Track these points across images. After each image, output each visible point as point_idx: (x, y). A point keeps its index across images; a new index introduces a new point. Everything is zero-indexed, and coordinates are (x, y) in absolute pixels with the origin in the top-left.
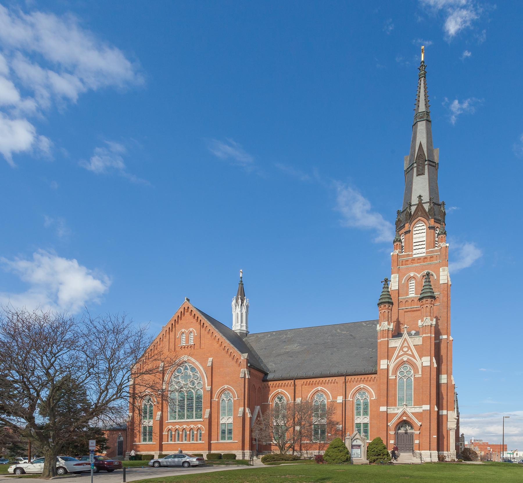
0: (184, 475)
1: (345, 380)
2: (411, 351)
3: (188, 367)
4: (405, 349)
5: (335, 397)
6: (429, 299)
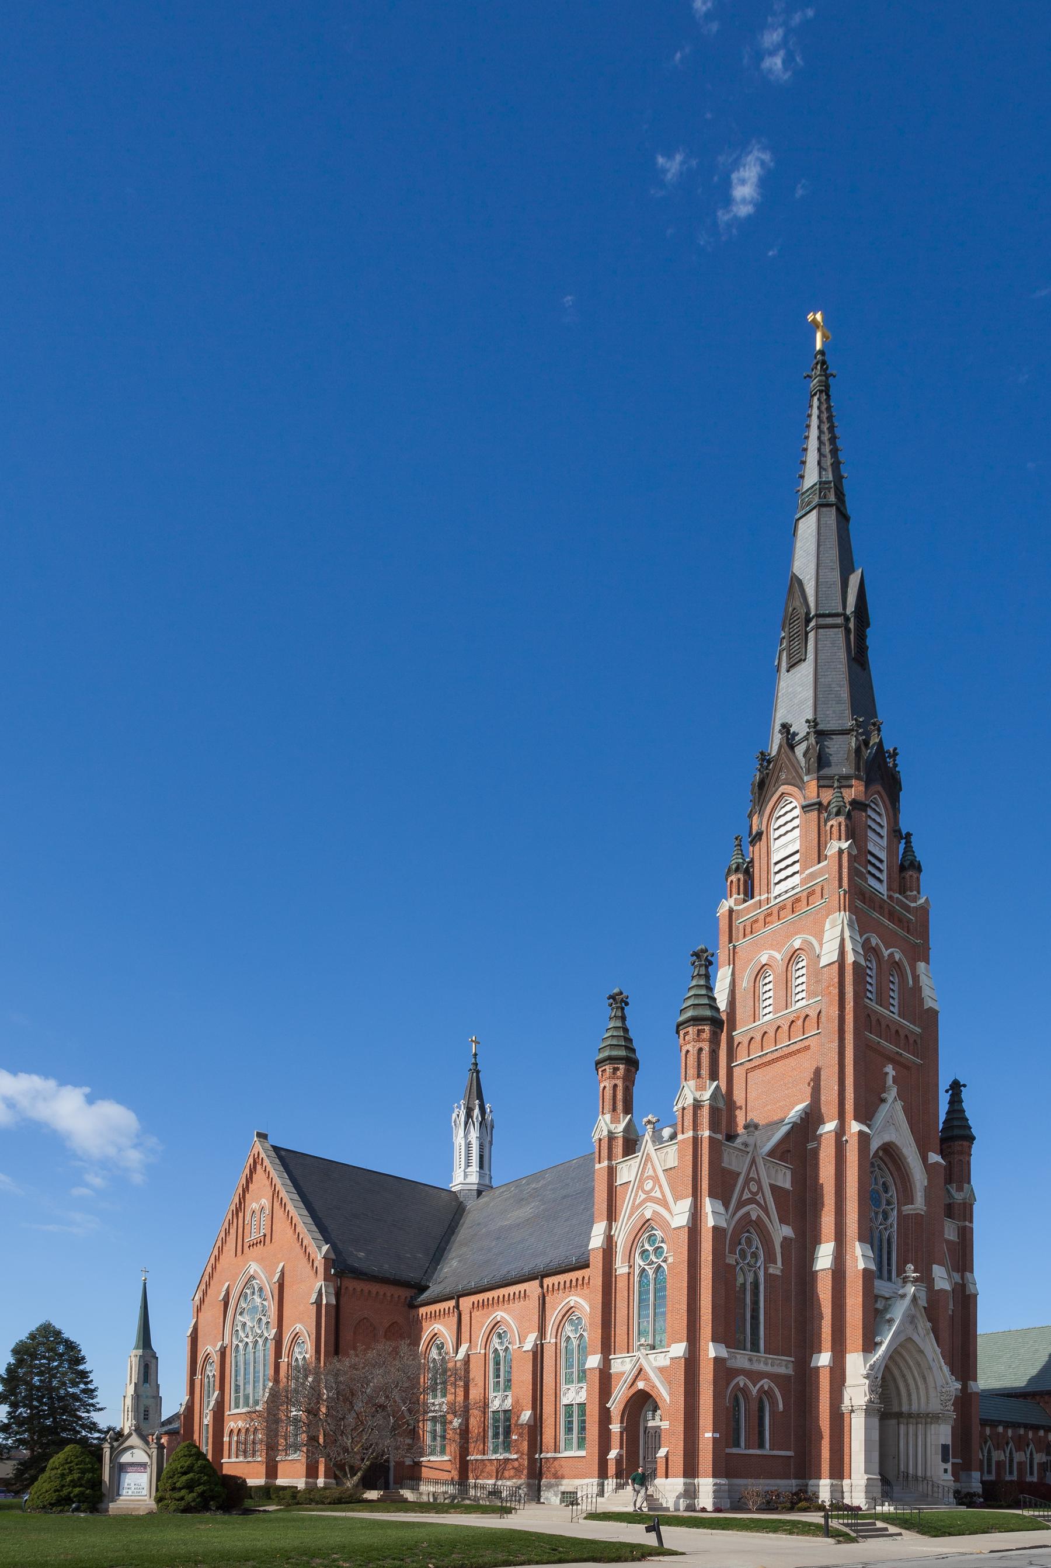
1: (542, 1286)
2: (660, 1186)
4: (649, 1185)
6: (690, 1029)
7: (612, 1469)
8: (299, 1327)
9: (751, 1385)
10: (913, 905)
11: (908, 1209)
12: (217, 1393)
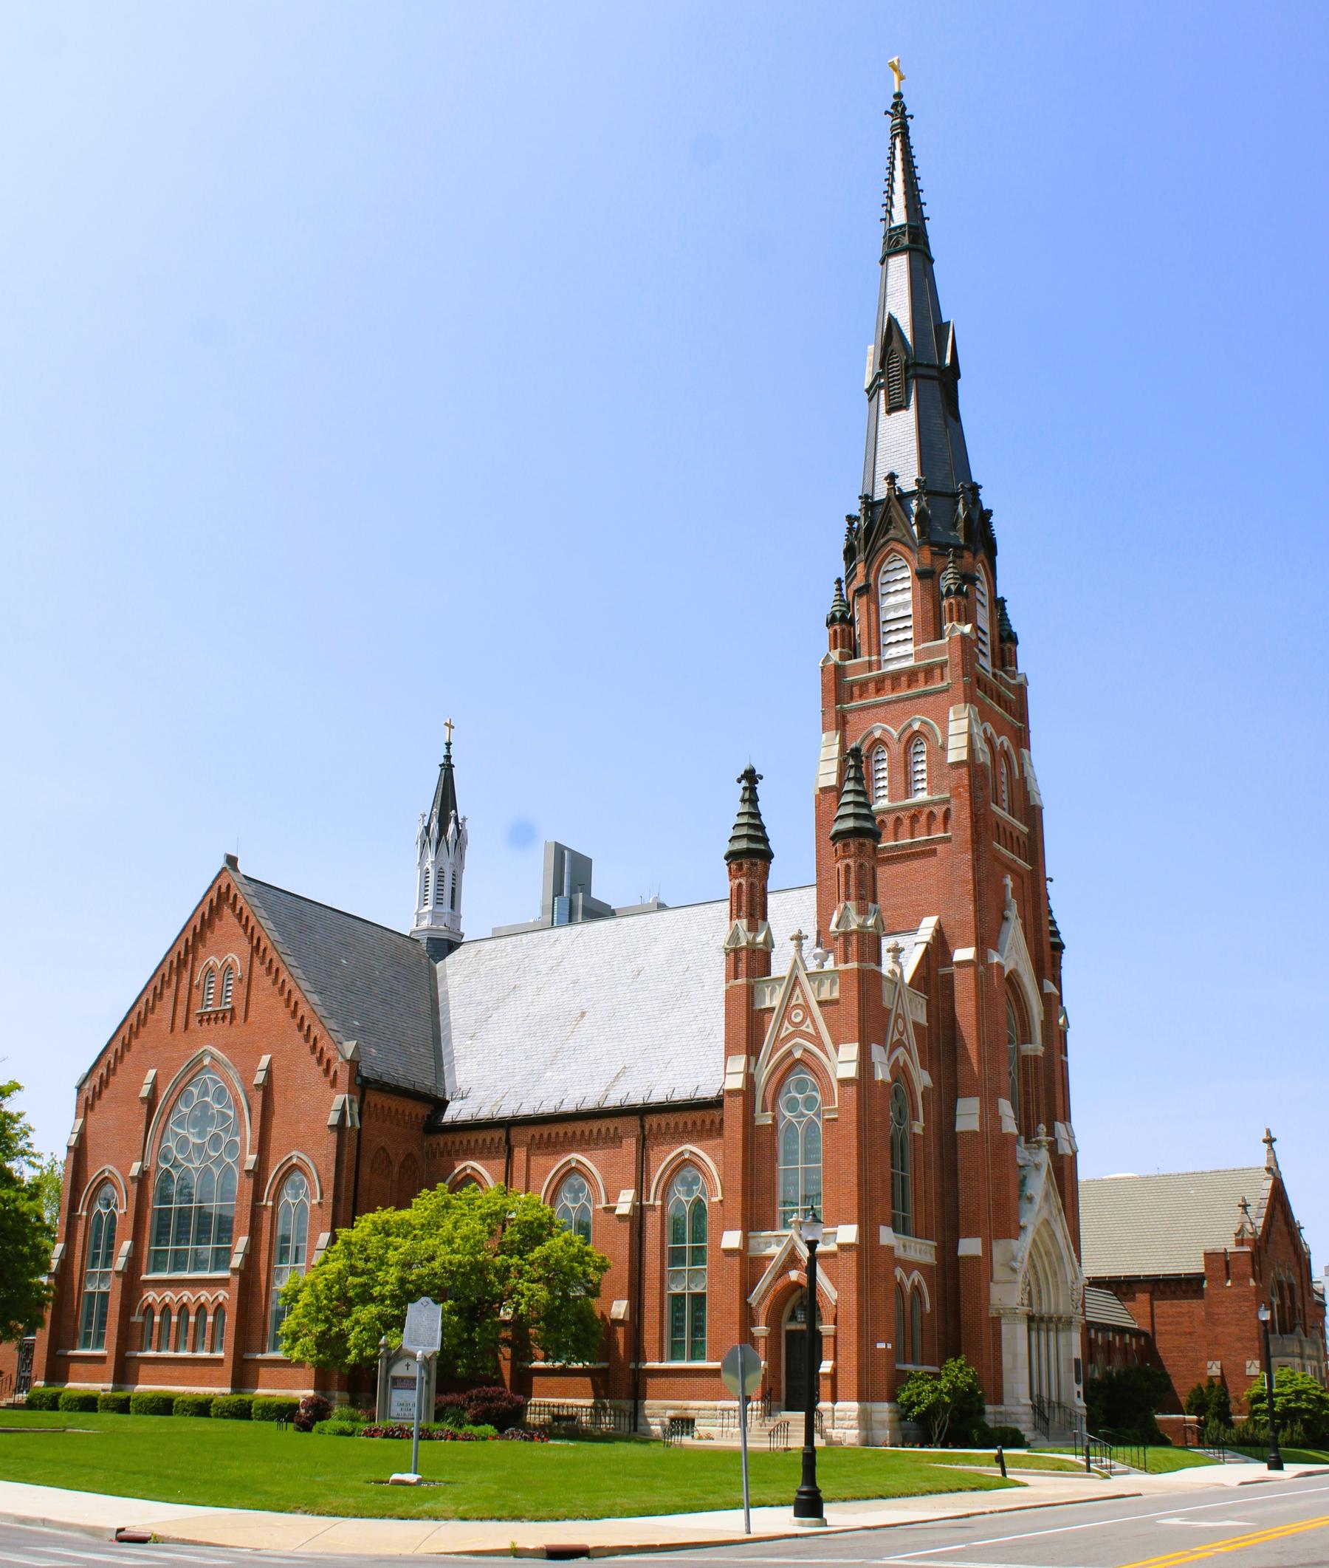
0: (312, 1506)
1: (643, 1127)
2: (813, 1021)
3: (210, 1085)
5: (612, 1196)
8: (296, 1156)
9: (905, 1278)
10: (1013, 682)
11: (1027, 1049)
12: (127, 1244)
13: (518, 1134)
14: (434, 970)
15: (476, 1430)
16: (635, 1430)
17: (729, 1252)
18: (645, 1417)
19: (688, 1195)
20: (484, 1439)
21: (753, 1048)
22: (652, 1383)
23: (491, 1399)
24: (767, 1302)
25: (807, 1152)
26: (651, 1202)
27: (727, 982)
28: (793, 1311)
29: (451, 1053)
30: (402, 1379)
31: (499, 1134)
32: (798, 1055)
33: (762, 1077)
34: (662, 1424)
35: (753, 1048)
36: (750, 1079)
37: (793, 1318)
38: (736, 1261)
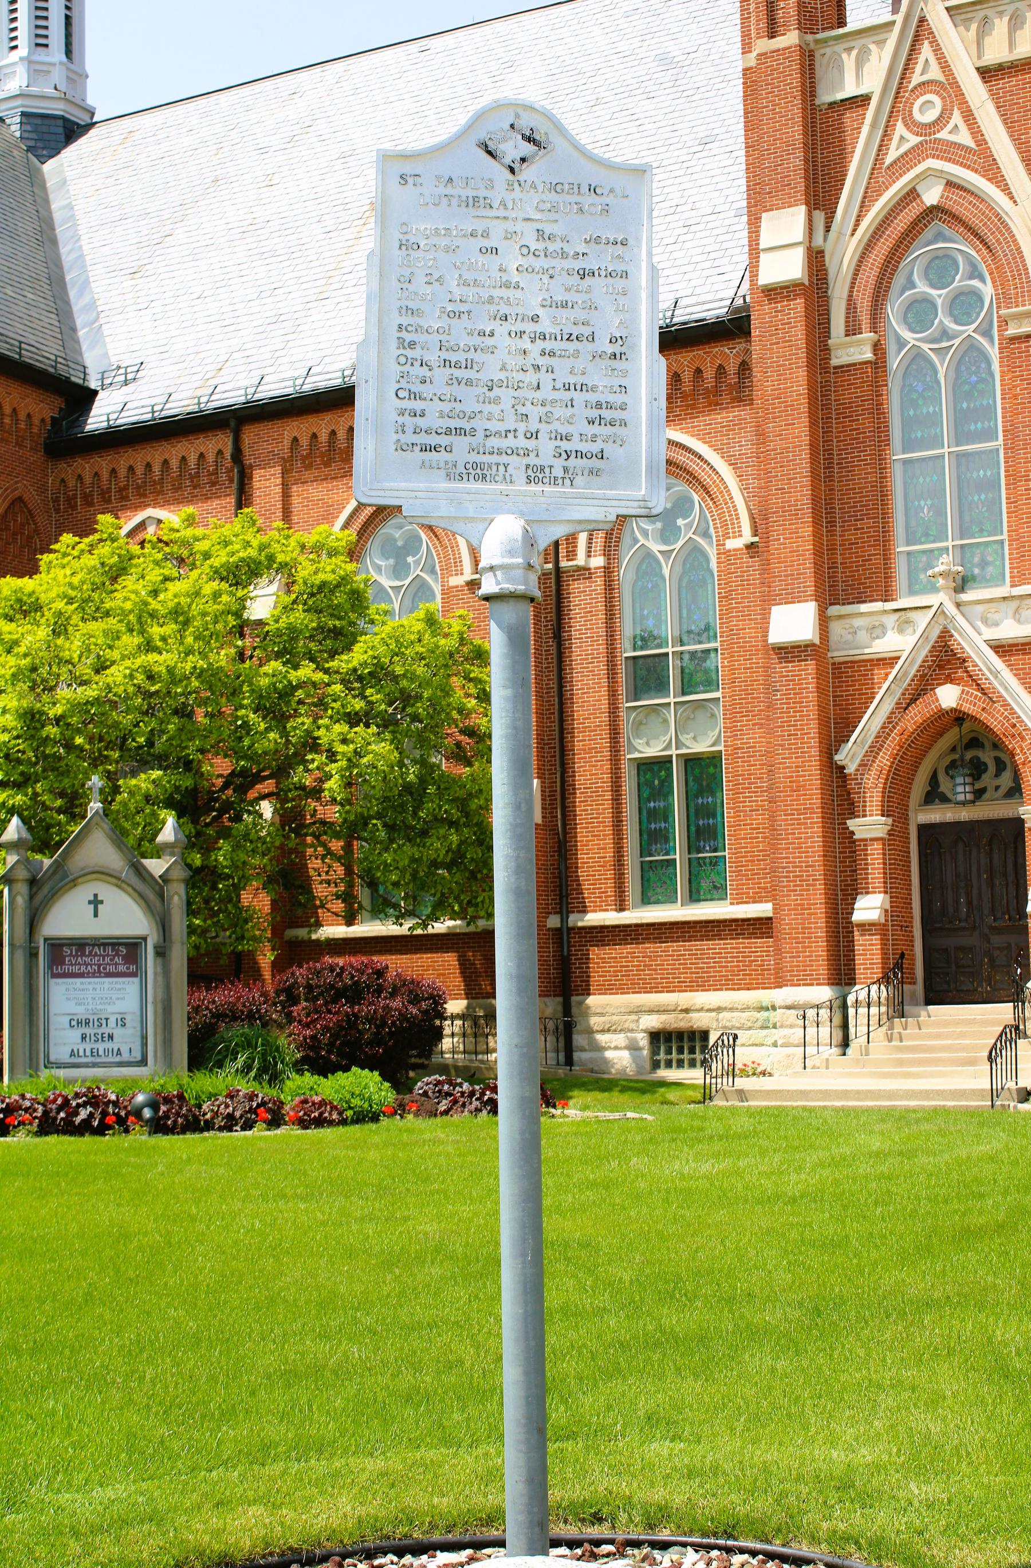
2: (969, 117)
4: (927, 109)
7: (868, 954)
13: (263, 441)
14: (39, 172)
15: (333, 1087)
16: (569, 1061)
17: (789, 652)
18: (590, 1032)
19: (665, 541)
20: (375, 1118)
21: (821, 193)
22: (602, 959)
23: (354, 993)
24: (884, 760)
25: (960, 419)
26: (581, 560)
27: (746, 48)
28: (934, 780)
29: (93, 305)
30: (81, 945)
31: (216, 445)
32: (931, 196)
33: (845, 253)
34: (633, 1047)
35: (821, 193)
36: (816, 260)
37: (933, 796)
38: (807, 672)
